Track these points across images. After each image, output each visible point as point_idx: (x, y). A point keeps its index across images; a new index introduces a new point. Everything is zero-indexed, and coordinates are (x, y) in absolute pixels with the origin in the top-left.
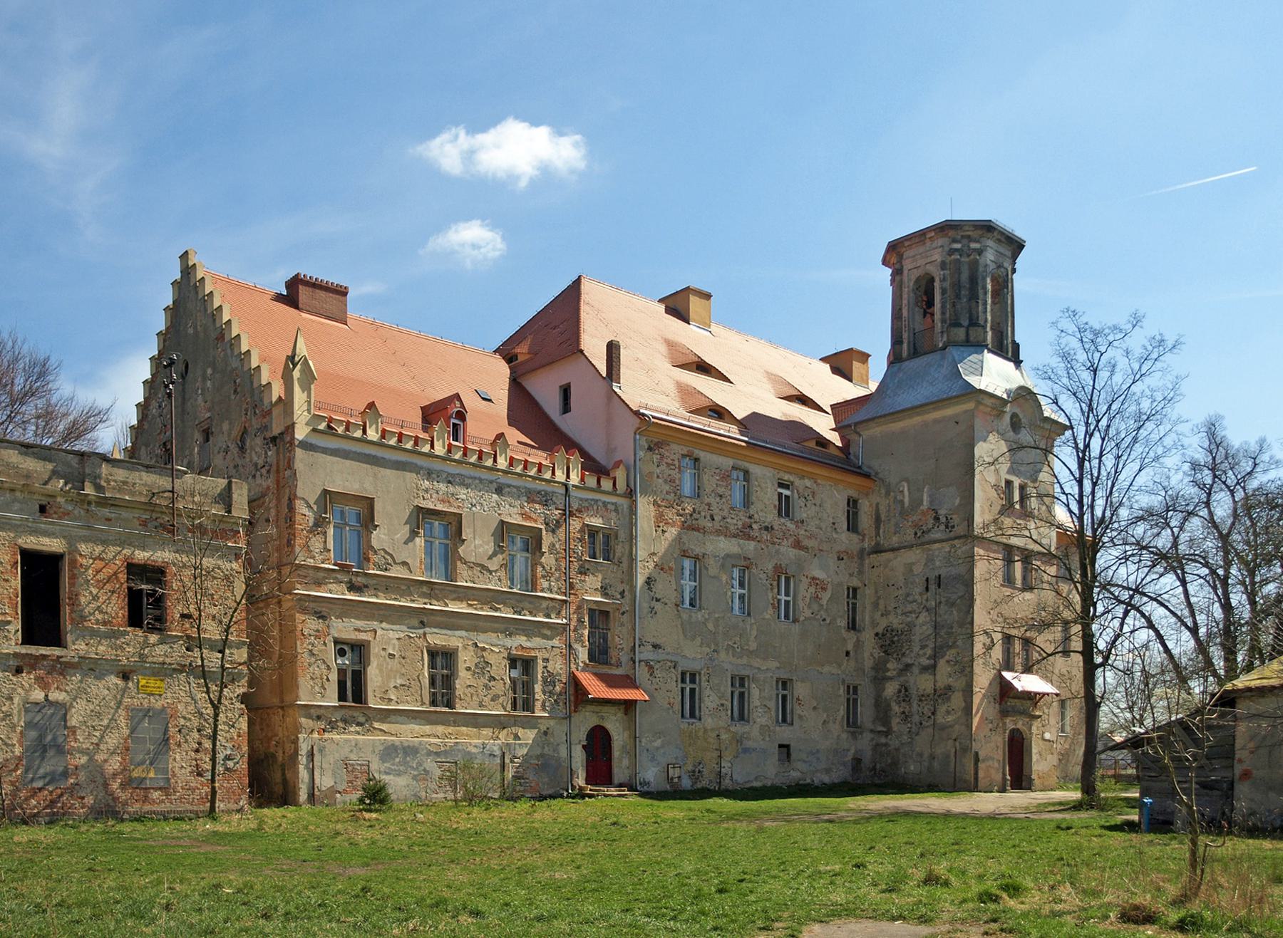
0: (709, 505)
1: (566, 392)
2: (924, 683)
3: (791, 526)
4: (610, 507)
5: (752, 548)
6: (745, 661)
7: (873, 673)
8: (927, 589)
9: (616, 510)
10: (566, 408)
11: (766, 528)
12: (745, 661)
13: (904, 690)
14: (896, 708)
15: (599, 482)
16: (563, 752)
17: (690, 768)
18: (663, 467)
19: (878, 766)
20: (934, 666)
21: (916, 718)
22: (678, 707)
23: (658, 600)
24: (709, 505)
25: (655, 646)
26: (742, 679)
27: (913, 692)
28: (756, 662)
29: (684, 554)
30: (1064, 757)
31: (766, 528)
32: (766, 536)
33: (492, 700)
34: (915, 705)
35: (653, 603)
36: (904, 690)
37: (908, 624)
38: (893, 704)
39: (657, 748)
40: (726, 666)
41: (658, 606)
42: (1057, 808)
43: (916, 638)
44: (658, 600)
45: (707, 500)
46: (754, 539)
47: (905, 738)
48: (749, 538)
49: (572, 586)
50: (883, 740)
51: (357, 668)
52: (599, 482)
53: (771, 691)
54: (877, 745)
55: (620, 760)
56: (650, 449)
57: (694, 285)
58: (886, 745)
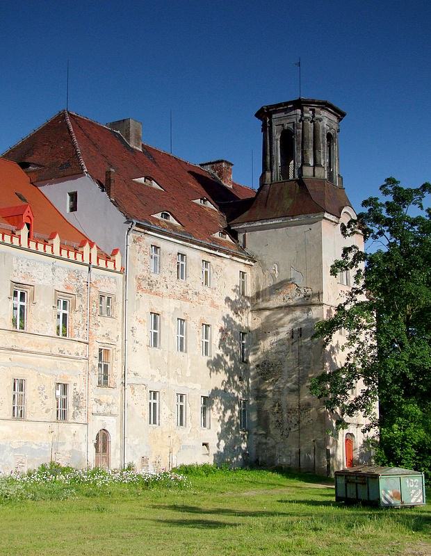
0: (165, 278)
2: (292, 401)
3: (209, 291)
4: (112, 280)
6: (183, 384)
7: (255, 393)
10: (74, 209)
12: (183, 384)
14: (272, 418)
16: (84, 449)
18: (141, 253)
19: (260, 459)
20: (298, 390)
21: (286, 426)
23: (137, 342)
24: (165, 278)
27: (284, 406)
28: (191, 385)
30: (117, 444)
32: (195, 298)
33: (46, 412)
35: (135, 344)
36: (277, 403)
37: (280, 360)
38: (271, 416)
41: (137, 346)
42: (179, 516)
43: (285, 369)
44: (137, 342)
46: (189, 300)
47: (279, 439)
53: (175, 402)
55: (115, 454)
58: (266, 444)
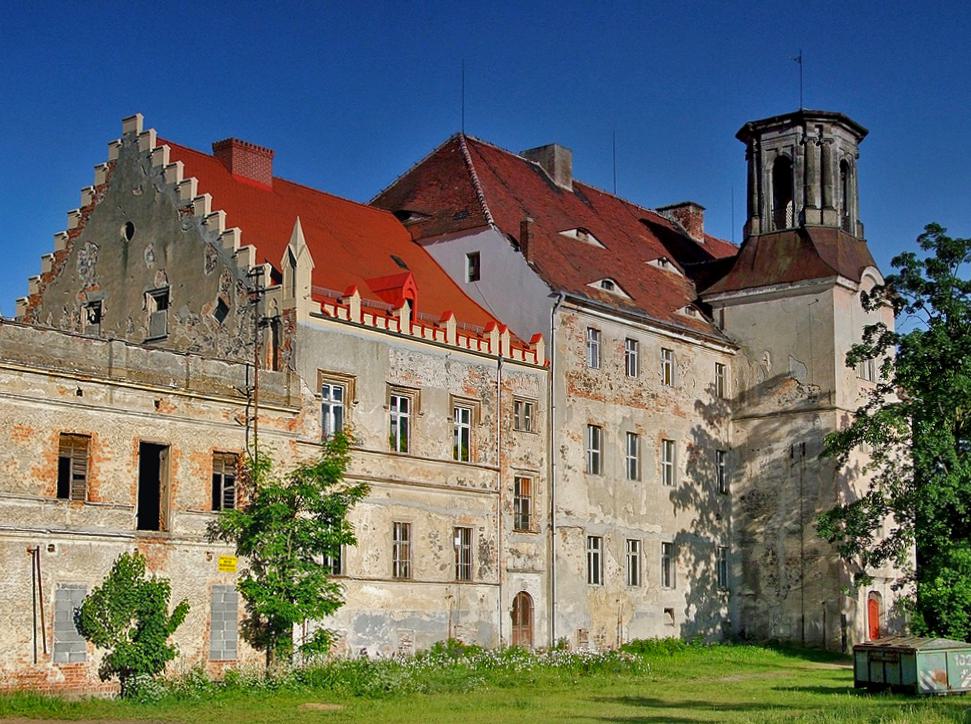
0: (608, 374)
1: (475, 259)
2: (792, 547)
3: (672, 393)
4: (532, 379)
5: (641, 415)
6: (637, 526)
8: (792, 456)
9: (537, 381)
10: (475, 277)
11: (653, 396)
12: (637, 526)
13: (771, 551)
14: (764, 572)
15: (434, 335)
16: (496, 620)
17: (595, 634)
18: (574, 340)
19: (747, 630)
20: (801, 531)
22: (585, 572)
23: (570, 468)
24: (608, 374)
25: (568, 513)
26: (634, 543)
28: (646, 527)
29: (664, 440)
31: (653, 396)
32: (652, 403)
33: (441, 569)
34: (783, 568)
39: (570, 614)
40: (623, 531)
41: (570, 473)
43: (782, 502)
44: (570, 468)
45: (607, 371)
46: (643, 406)
48: (640, 405)
49: (502, 455)
50: (752, 604)
51: (466, 547)
52: (434, 335)
54: (746, 608)
56: (564, 323)
57: (691, 201)
58: (755, 608)
